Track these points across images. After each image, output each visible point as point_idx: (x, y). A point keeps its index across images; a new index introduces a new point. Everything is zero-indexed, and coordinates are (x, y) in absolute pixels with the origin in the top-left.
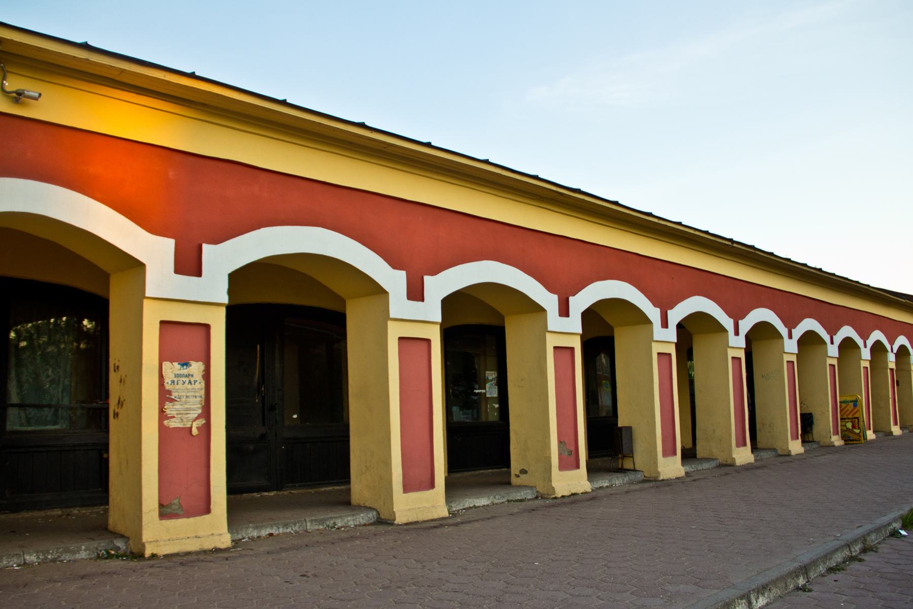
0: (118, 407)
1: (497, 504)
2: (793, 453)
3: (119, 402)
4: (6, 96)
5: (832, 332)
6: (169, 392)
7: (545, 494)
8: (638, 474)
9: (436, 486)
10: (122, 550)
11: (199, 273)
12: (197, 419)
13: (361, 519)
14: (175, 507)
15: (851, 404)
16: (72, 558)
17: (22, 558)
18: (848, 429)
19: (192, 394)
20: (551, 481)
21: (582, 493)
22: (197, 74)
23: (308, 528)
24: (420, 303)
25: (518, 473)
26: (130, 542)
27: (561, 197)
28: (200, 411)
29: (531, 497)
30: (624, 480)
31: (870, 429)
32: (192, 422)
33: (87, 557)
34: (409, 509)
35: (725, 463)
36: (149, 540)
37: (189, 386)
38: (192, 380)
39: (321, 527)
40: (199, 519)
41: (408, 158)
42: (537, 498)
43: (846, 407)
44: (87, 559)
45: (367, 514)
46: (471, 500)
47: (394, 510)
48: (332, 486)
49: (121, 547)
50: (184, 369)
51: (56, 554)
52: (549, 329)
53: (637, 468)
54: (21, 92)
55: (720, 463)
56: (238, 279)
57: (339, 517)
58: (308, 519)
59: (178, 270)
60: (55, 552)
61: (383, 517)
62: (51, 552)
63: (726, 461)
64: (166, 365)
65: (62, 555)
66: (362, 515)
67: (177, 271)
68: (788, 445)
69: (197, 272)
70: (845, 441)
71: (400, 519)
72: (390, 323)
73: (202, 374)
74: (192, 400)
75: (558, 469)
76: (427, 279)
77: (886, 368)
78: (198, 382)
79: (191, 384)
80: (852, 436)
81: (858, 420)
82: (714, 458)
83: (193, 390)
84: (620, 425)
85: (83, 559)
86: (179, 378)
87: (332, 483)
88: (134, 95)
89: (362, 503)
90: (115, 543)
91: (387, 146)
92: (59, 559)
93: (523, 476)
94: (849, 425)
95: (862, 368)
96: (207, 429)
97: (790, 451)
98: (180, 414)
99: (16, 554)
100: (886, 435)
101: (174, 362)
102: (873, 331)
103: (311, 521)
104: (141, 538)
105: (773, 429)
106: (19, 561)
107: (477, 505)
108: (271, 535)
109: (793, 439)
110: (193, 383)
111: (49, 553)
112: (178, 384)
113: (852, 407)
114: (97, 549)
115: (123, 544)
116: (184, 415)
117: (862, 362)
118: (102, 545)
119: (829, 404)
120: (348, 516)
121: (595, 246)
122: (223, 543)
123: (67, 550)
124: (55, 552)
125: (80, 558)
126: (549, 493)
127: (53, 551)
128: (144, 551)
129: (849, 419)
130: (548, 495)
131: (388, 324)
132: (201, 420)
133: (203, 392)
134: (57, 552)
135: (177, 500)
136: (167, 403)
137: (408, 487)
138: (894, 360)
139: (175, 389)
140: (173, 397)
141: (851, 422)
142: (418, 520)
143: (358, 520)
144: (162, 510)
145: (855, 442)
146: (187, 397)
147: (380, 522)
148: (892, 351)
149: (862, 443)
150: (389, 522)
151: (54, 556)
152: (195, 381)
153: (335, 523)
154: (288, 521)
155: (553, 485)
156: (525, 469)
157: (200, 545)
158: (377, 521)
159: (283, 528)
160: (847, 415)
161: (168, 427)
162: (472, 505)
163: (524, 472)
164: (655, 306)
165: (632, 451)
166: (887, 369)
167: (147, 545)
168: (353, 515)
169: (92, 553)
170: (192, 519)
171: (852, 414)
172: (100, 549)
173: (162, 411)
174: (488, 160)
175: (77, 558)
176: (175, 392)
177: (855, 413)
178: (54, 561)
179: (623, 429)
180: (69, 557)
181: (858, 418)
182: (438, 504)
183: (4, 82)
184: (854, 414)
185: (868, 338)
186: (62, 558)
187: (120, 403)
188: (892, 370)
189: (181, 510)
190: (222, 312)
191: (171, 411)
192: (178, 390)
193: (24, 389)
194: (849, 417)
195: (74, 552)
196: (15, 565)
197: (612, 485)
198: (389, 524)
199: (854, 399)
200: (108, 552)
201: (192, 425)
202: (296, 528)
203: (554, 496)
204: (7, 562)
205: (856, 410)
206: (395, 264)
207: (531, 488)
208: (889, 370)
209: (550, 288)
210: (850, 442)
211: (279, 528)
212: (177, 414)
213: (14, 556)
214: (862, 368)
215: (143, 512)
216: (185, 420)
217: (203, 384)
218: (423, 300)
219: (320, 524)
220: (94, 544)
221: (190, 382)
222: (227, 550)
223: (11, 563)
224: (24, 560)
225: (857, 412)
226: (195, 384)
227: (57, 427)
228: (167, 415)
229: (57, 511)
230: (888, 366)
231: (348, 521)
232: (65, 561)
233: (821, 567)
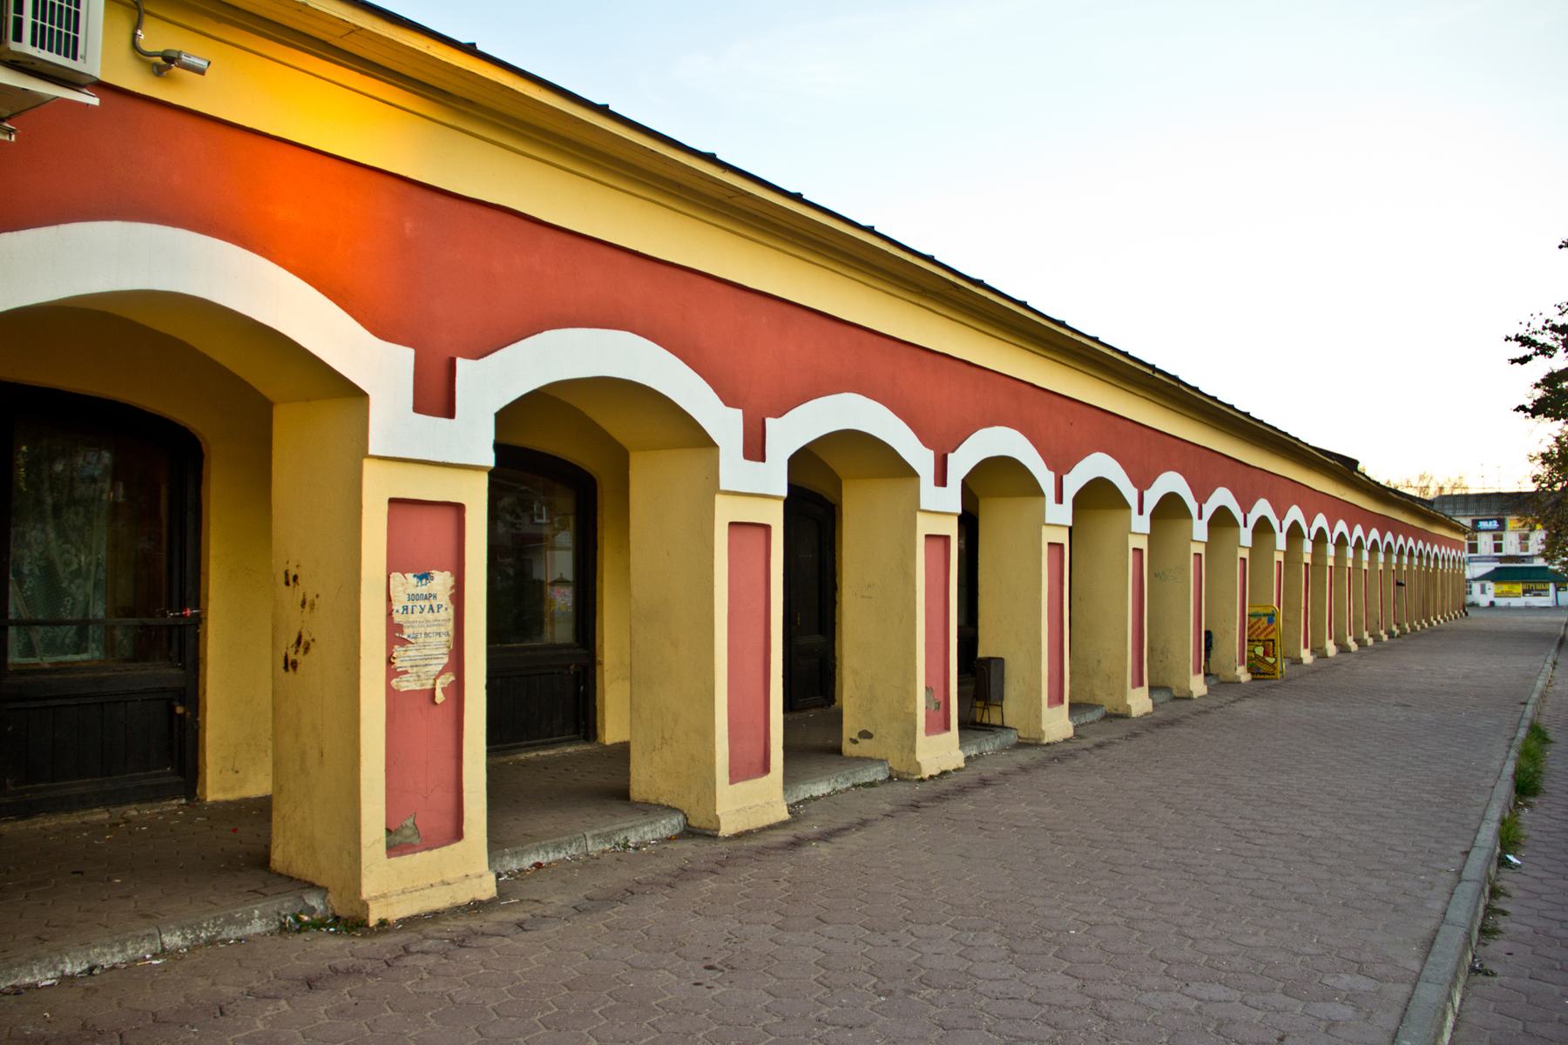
0: (296, 652)
1: (840, 791)
3: (299, 642)
4: (141, 60)
5: (1142, 482)
6: (400, 628)
7: (904, 773)
8: (1011, 733)
9: (771, 769)
10: (318, 912)
11: (450, 412)
12: (441, 673)
13: (662, 828)
14: (407, 832)
15: (1265, 620)
16: (240, 934)
17: (159, 941)
18: (1257, 656)
19: (435, 629)
20: (914, 752)
21: (954, 770)
22: (480, 47)
23: (589, 849)
24: (761, 464)
25: (855, 736)
26: (330, 896)
27: (954, 293)
28: (446, 660)
29: (883, 778)
30: (994, 744)
32: (435, 680)
33: (264, 929)
34: (738, 811)
35: (1115, 712)
36: (373, 894)
37: (430, 616)
38: (435, 603)
39: (608, 846)
40: (445, 849)
42: (890, 778)
43: (1255, 623)
44: (265, 935)
45: (671, 819)
46: (804, 787)
47: (717, 813)
48: (535, 750)
49: (316, 907)
50: (422, 585)
51: (213, 928)
52: (922, 507)
53: (1007, 723)
54: (175, 56)
55: (1106, 712)
56: (506, 418)
57: (632, 827)
58: (588, 834)
60: (211, 925)
61: (693, 823)
62: (205, 925)
63: (1117, 710)
64: (396, 577)
65: (223, 930)
66: (663, 822)
68: (1189, 682)
70: (1252, 674)
71: (728, 826)
72: (719, 499)
73: (450, 593)
74: (434, 640)
75: (924, 733)
76: (770, 422)
77: (1300, 562)
78: (443, 609)
79: (433, 612)
80: (1264, 668)
81: (1274, 643)
82: (1097, 703)
83: (436, 623)
84: (981, 654)
85: (259, 934)
86: (415, 602)
87: (535, 745)
88: (356, 74)
89: (652, 799)
90: (307, 901)
91: (734, 194)
92: (219, 938)
93: (865, 743)
94: (1260, 651)
95: (1275, 563)
96: (457, 690)
97: (1191, 692)
98: (416, 666)
99: (148, 935)
100: (1292, 664)
101: (408, 572)
103: (593, 837)
104: (358, 892)
105: (1167, 657)
106: (153, 948)
107: (815, 794)
108: (538, 866)
109: (1194, 673)
110: (435, 609)
111: (203, 928)
112: (412, 613)
113: (1266, 624)
114: (279, 914)
115: (319, 901)
116: (421, 668)
118: (286, 905)
119: (1236, 618)
120: (643, 825)
121: (984, 372)
122: (485, 890)
123: (230, 921)
124: (211, 925)
125: (253, 932)
126: (910, 771)
127: (208, 924)
128: (368, 916)
129: (1260, 641)
130: (909, 774)
131: (716, 500)
132: (447, 675)
133: (450, 626)
134: (215, 925)
135: (412, 820)
136: (396, 647)
137: (736, 776)
138: (1311, 551)
139: (409, 622)
140: (405, 636)
141: (1263, 646)
142: (751, 828)
143: (658, 830)
144: (389, 838)
145: (1267, 676)
146: (427, 635)
147: (690, 832)
148: (1309, 537)
149: (1277, 679)
150: (708, 832)
151: (211, 932)
152: (439, 607)
153: (626, 838)
154: (561, 839)
155: (918, 759)
156: (869, 730)
157: (451, 897)
158: (685, 830)
159: (554, 852)
160: (1256, 636)
161: (398, 690)
162: (808, 796)
163: (865, 735)
164: (1049, 469)
165: (1001, 698)
166: (1301, 563)
167: (372, 906)
168: (652, 823)
169: (270, 922)
170: (435, 852)
171: (1265, 633)
172: (284, 913)
174: (873, 227)
175: (248, 932)
176: (409, 627)
177: (1270, 633)
178: (211, 942)
179: (993, 662)
180: (234, 933)
181: (1273, 641)
182: (774, 799)
183: (139, 32)
184: (1267, 635)
185: (1284, 519)
186: (224, 936)
188: (1307, 565)
189: (417, 836)
190: (483, 481)
191: (402, 661)
192: (413, 624)
193: (26, 587)
194: (1260, 638)
195: (243, 923)
196: (148, 956)
197: (982, 753)
198: (709, 836)
199: (1269, 611)
200: (298, 919)
201: (434, 684)
202: (572, 851)
203: (919, 777)
204: (134, 951)
205: (1272, 627)
206: (729, 400)
207: (881, 761)
208: (1303, 566)
210: (1259, 676)
211: (547, 853)
212: (412, 666)
213: (144, 939)
214: (1275, 563)
215: (362, 846)
216: (423, 676)
217: (451, 611)
218: (763, 460)
219: (605, 841)
220: (273, 905)
221: (431, 608)
222: (491, 902)
223: (141, 951)
224: (162, 944)
225: (1272, 631)
226: (438, 612)
227: (85, 656)
228: (395, 669)
229: (100, 813)
230: (1302, 558)
231: (644, 833)
232: (232, 941)
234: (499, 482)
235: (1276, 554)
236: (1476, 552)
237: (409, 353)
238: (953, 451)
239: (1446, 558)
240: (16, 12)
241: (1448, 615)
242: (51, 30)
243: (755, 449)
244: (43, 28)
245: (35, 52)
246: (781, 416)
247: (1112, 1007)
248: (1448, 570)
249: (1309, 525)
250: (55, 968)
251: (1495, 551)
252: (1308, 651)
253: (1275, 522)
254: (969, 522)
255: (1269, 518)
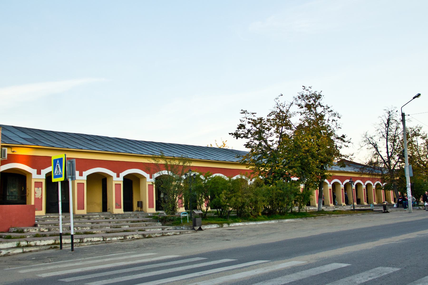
2: (76, 214)
59: (37, 174)
64: (35, 188)
67: (37, 174)
69: (40, 174)
96: (42, 198)
128: (146, 210)
133: (41, 192)
173: (35, 195)
187: (28, 194)
192: (37, 192)
214: (329, 190)
218: (82, 176)
248: (191, 231)
250: (280, 182)
252: (393, 202)
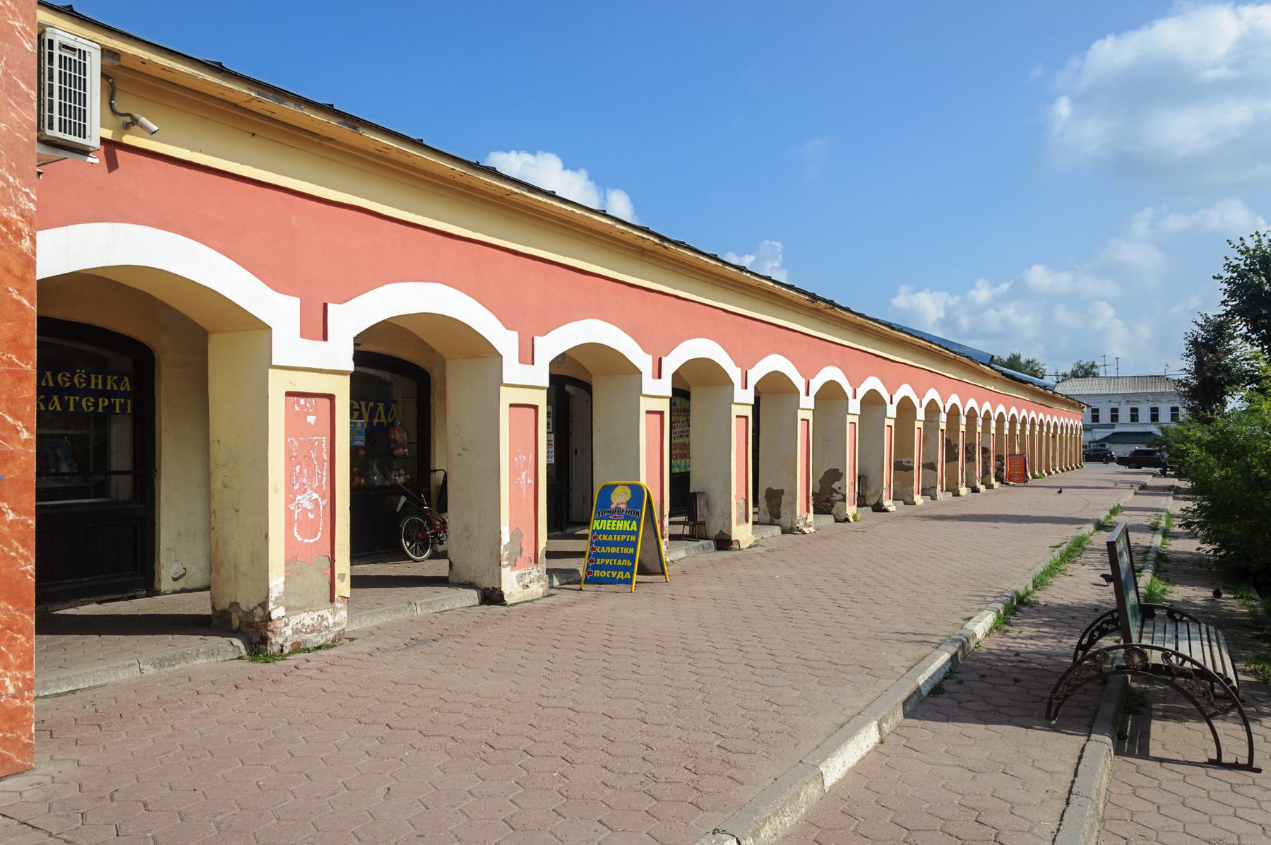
31: (918, 493)
41: (526, 206)
102: (928, 390)
117: (886, 419)
148: (944, 411)
164: (737, 366)
190: (346, 380)
209: (646, 349)
230: (939, 426)
233: (1265, 473)
234: (357, 380)
235: (941, 424)
236: (1098, 421)
237: (297, 301)
238: (666, 356)
239: (1064, 426)
240: (49, 49)
241: (1071, 466)
242: (70, 90)
243: (527, 356)
244: (65, 73)
245: (61, 135)
246: (544, 335)
247: (712, 688)
249: (945, 402)
251: (1093, 421)
253: (916, 401)
254: (756, 408)
255: (936, 400)
